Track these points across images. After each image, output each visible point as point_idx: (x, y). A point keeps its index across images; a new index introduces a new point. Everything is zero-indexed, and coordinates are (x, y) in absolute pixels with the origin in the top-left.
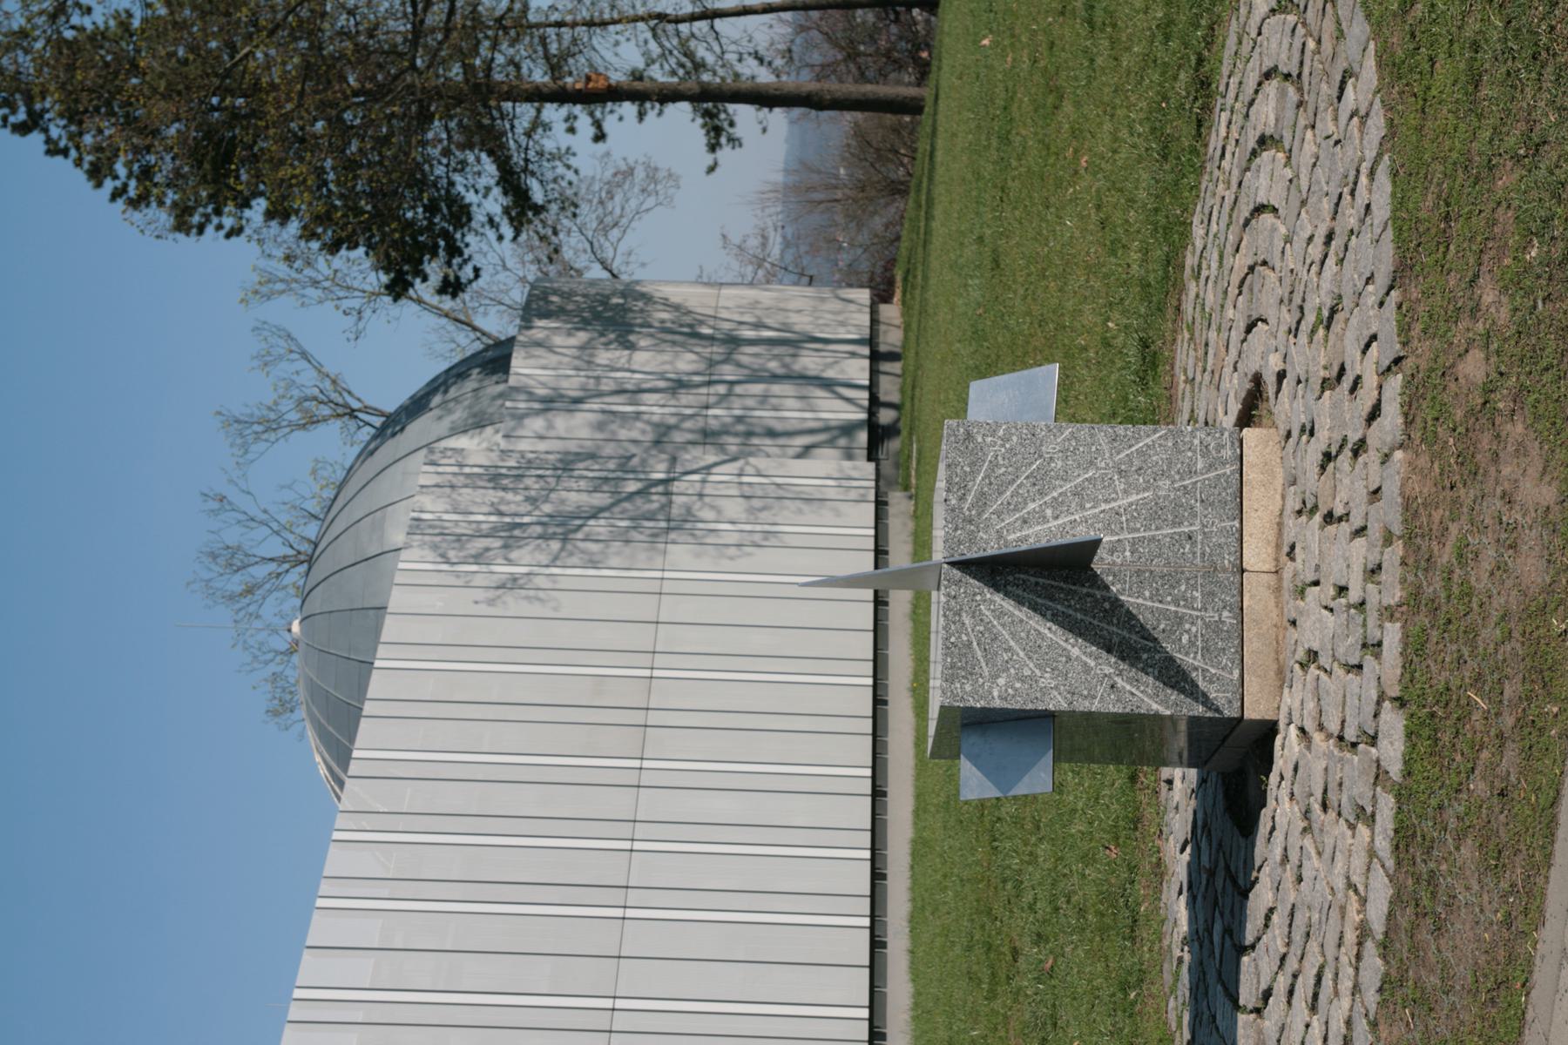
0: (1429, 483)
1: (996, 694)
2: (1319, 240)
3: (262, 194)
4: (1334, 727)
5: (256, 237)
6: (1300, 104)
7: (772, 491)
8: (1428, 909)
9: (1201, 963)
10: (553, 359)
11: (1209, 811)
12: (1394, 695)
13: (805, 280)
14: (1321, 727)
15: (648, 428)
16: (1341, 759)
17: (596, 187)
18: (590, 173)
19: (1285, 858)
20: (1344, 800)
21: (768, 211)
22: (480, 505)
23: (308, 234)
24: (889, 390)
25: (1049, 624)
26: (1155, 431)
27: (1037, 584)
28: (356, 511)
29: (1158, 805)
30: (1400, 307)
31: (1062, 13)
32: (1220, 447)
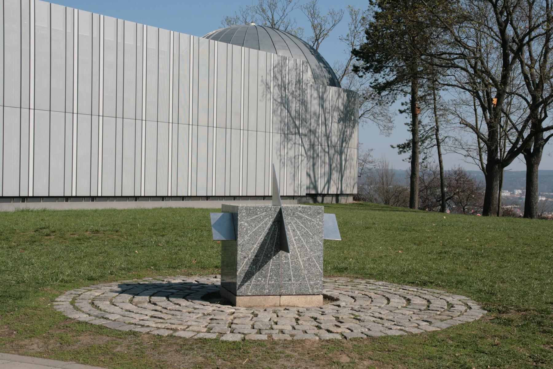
0: (309, 347)
1: (242, 222)
2: (380, 316)
3: (383, 11)
4: (235, 321)
5: (370, 9)
6: (420, 310)
7: (297, 165)
8: (183, 348)
9: (163, 286)
10: (335, 99)
11: (208, 288)
12: (246, 338)
13: (360, 175)
14: (235, 318)
15: (315, 128)
16: (226, 323)
17: (386, 112)
18: (390, 110)
19: (195, 309)
20: (214, 325)
21: (380, 163)
22: (291, 78)
23: (371, 25)
24: (327, 200)
25: (263, 238)
26: (321, 269)
27: (275, 234)
28: (289, 42)
29: (209, 274)
30: (362, 338)
31: (443, 245)
32: (317, 288)
